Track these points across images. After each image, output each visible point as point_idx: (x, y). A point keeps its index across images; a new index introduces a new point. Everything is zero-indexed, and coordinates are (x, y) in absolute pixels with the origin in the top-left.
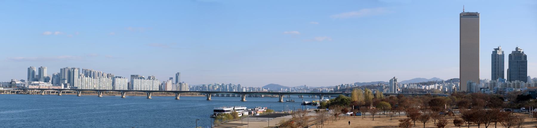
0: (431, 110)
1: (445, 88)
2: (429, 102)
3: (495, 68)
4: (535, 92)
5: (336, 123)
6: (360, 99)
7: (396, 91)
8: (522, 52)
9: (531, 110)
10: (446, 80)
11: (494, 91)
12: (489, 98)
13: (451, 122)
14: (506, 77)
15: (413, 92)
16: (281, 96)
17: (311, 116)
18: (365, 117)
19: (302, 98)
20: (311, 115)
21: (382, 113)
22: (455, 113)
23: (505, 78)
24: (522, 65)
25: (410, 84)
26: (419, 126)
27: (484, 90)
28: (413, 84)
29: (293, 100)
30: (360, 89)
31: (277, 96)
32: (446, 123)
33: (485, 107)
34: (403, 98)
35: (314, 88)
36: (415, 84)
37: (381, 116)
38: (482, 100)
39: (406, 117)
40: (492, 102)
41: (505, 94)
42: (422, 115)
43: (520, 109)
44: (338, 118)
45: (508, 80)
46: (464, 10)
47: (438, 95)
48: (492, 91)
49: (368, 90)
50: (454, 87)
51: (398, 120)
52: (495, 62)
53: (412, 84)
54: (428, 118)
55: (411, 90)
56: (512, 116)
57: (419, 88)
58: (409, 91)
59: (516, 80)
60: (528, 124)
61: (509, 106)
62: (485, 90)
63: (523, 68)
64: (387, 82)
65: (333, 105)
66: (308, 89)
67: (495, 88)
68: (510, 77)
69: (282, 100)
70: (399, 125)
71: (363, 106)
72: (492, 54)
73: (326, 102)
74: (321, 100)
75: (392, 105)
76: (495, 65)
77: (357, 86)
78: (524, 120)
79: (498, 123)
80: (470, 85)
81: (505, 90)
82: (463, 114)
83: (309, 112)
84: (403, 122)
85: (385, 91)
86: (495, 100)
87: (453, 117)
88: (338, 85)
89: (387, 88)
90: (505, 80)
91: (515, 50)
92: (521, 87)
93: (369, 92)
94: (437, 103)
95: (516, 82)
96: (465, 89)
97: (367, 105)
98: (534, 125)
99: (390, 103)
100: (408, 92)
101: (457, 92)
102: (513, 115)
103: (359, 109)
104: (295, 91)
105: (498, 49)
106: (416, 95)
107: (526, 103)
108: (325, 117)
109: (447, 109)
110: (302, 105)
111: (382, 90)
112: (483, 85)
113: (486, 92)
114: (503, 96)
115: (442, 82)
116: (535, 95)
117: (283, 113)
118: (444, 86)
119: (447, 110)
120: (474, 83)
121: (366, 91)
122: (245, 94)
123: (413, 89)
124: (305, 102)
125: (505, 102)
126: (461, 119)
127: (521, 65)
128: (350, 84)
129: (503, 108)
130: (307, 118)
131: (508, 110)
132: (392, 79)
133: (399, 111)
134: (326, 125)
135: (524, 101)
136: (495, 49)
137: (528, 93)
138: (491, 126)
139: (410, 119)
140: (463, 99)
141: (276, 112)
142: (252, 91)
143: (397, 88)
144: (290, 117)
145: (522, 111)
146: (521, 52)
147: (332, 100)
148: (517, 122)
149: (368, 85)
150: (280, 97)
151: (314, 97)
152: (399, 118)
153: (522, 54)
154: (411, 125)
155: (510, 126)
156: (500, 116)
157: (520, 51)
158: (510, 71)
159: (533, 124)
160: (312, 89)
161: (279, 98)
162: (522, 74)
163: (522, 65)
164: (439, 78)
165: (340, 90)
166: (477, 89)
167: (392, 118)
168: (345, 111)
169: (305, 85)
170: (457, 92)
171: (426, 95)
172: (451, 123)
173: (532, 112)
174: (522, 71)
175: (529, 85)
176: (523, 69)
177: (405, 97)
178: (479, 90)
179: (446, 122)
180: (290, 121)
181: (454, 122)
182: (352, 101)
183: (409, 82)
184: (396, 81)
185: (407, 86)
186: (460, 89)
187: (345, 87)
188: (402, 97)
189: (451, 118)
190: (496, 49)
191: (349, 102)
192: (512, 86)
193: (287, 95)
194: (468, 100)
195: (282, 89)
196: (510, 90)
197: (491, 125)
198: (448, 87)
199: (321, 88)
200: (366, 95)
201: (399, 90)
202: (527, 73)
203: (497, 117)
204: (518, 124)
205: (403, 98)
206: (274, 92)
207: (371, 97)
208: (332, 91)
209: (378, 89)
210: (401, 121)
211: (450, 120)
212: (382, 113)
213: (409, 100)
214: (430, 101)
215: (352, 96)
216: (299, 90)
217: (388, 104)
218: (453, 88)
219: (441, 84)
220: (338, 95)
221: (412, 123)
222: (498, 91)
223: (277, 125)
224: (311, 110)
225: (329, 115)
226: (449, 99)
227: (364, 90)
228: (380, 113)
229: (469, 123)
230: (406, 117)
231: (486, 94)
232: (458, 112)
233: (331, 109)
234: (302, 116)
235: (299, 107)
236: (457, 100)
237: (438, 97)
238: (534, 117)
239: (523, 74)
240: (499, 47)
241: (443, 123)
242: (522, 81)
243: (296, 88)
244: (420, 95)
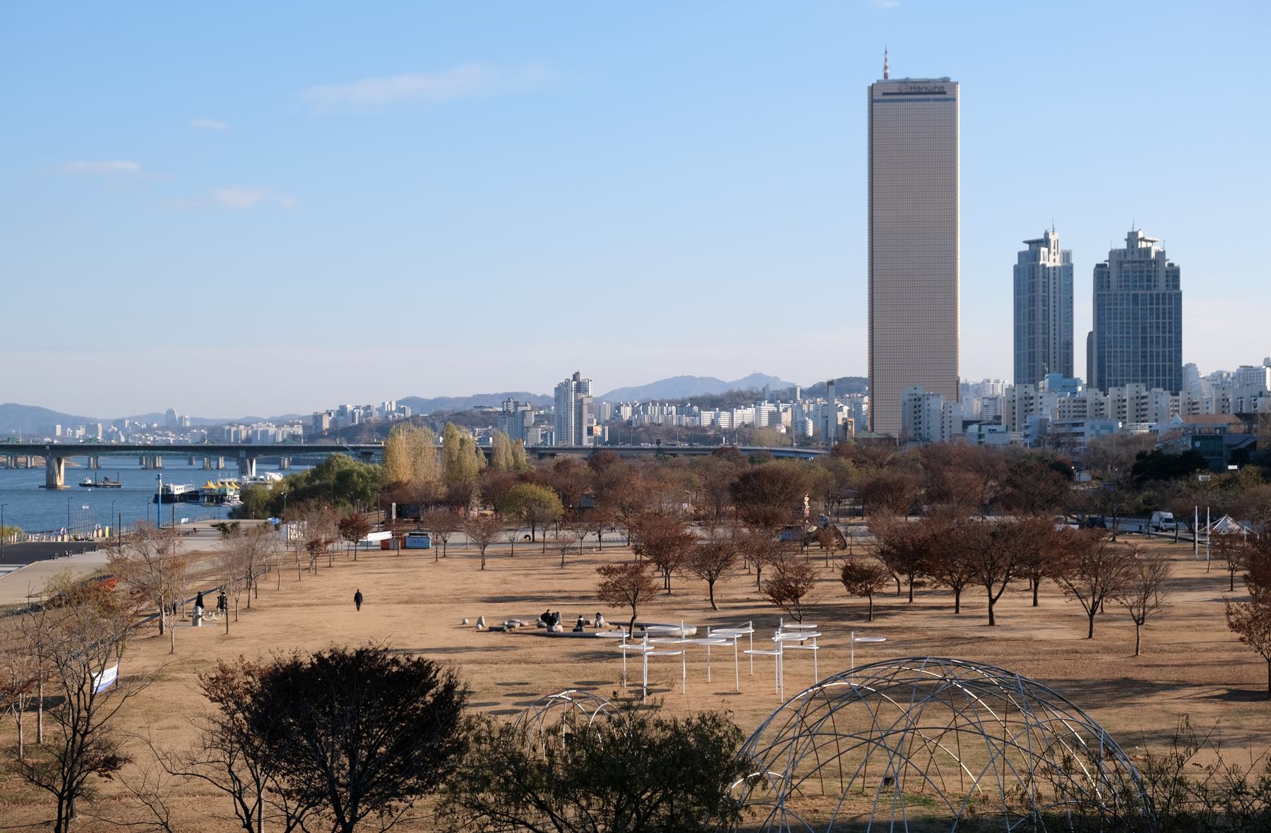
0: (740, 521)
1: (804, 424)
2: (732, 485)
3: (1032, 330)
4: (1220, 438)
5: (314, 585)
6: (423, 471)
7: (585, 437)
8: (1158, 253)
9: (1203, 521)
10: (806, 382)
11: (1026, 436)
12: (1002, 466)
13: (831, 576)
14: (1080, 369)
15: (658, 442)
16: (55, 461)
17: (197, 555)
18: (445, 556)
19: (155, 468)
20: (197, 548)
21: (524, 534)
22: (850, 535)
23: (1075, 376)
24: (1158, 314)
25: (645, 405)
26: (687, 594)
27: (980, 429)
28: (662, 404)
29: (113, 479)
30: (425, 428)
31: (37, 461)
32: (811, 580)
33: (986, 509)
34: (617, 468)
35: (213, 424)
36: (671, 403)
37: (517, 549)
38: (971, 476)
39: (629, 555)
40: (1015, 487)
41: (1077, 449)
42: (699, 543)
43: (1150, 518)
44: (322, 561)
45: (1089, 384)
46: (886, 68)
47: (773, 454)
48: (1016, 436)
49: (459, 429)
50: (842, 416)
51: (593, 567)
52: (1032, 302)
53: (654, 403)
54: (725, 559)
55: (652, 430)
56: (1113, 550)
57: (686, 420)
58: (644, 435)
59: (1128, 381)
60: (1190, 590)
61: (1097, 502)
62: (985, 429)
63: (1164, 328)
64: (544, 397)
65: (301, 500)
66: (185, 430)
67: (1033, 418)
68: (1101, 370)
69: (60, 482)
70: (599, 588)
71: (438, 503)
72: (1015, 267)
73: (270, 488)
74: (246, 479)
75: (565, 499)
76: (1032, 316)
77: (409, 413)
78: (1166, 570)
79: (1047, 583)
80: (916, 407)
81: (1144, 407)
82: (886, 542)
83: (187, 534)
84: (615, 578)
85: (536, 437)
86: (1030, 478)
87: (839, 553)
88: (322, 410)
89: (542, 422)
90: (1077, 382)
91: (1124, 246)
92: (1154, 417)
93: (462, 441)
94: (767, 491)
95: (1129, 391)
96: (892, 425)
97: (456, 499)
98: (1217, 595)
99: (557, 490)
100: (637, 440)
101: (856, 440)
102: (1119, 546)
103: (417, 520)
104: (123, 439)
105: (1045, 242)
106: (675, 455)
107: (1180, 491)
108: (265, 556)
109: (813, 519)
110: (156, 501)
111: (520, 431)
112: (974, 408)
113: (988, 439)
114: (1068, 456)
115: (788, 395)
116: (1221, 454)
117: (65, 541)
118: (799, 414)
119: (812, 521)
120: (932, 400)
121: (449, 437)
122: (66, 454)
123: (660, 425)
124: (168, 489)
125: (1079, 483)
126: (873, 562)
127: (1151, 313)
128: (376, 404)
129: (1068, 512)
130: (177, 564)
131: (1092, 523)
132: (567, 383)
133: (599, 524)
134: (271, 591)
135: (1167, 483)
136: (1030, 243)
137: (1186, 444)
138: (1014, 595)
139: (647, 562)
140: (885, 471)
141: (33, 539)
142: (123, 439)
143: (591, 421)
144: (99, 559)
145: (1157, 529)
146: (1153, 255)
147: (298, 479)
148: (1134, 577)
149: (460, 408)
150: (48, 464)
151: (214, 464)
152: (599, 557)
153: (1155, 262)
154: (651, 590)
155: (1101, 597)
156: (1054, 552)
157: (1148, 250)
158: (1098, 343)
159: (1211, 589)
160: (202, 427)
161: (48, 472)
162: (1158, 356)
163: (1158, 314)
164: (776, 379)
165: (333, 433)
166: (946, 425)
167: (568, 558)
168: (354, 529)
169: (171, 412)
170: (856, 440)
171: (719, 453)
172: (832, 580)
173: (1205, 535)
174: (1158, 343)
175: (1192, 407)
176: (1164, 332)
177: (627, 463)
178: (958, 428)
179: (808, 575)
180: (100, 579)
181: (843, 576)
182: (386, 484)
183: (643, 397)
184: (586, 391)
185: (635, 411)
186: (872, 424)
187: (353, 420)
188: (610, 461)
189: (833, 558)
190: (1036, 244)
191: (375, 485)
192: (1109, 410)
193: (86, 457)
194: (910, 476)
195: (59, 428)
196: (1103, 427)
197: (1012, 590)
198: (815, 418)
199: (247, 425)
200: (450, 454)
201: (598, 430)
202: (1180, 351)
203: (1041, 553)
204: (1139, 589)
205: (617, 468)
206: (21, 441)
207: (474, 463)
208: (294, 437)
209: (506, 428)
210: (608, 571)
211: (827, 567)
212: (520, 536)
213: (641, 475)
214: (736, 480)
215: (385, 461)
216: (143, 432)
217: (549, 495)
218: (840, 422)
219: (785, 402)
220: (321, 457)
221: (655, 582)
222: (1042, 435)
223: (36, 596)
224: (197, 526)
225: (282, 547)
226: (821, 471)
227: (442, 434)
228: (511, 534)
229: (911, 579)
230: (629, 555)
231: (987, 447)
232: (864, 528)
233: (293, 520)
234: (153, 554)
235: (141, 511)
236: (857, 476)
237: (773, 463)
238: (1215, 556)
239: (1164, 356)
240: (1046, 234)
241: (797, 582)
242: (1158, 386)
243: (127, 422)
244: (691, 452)
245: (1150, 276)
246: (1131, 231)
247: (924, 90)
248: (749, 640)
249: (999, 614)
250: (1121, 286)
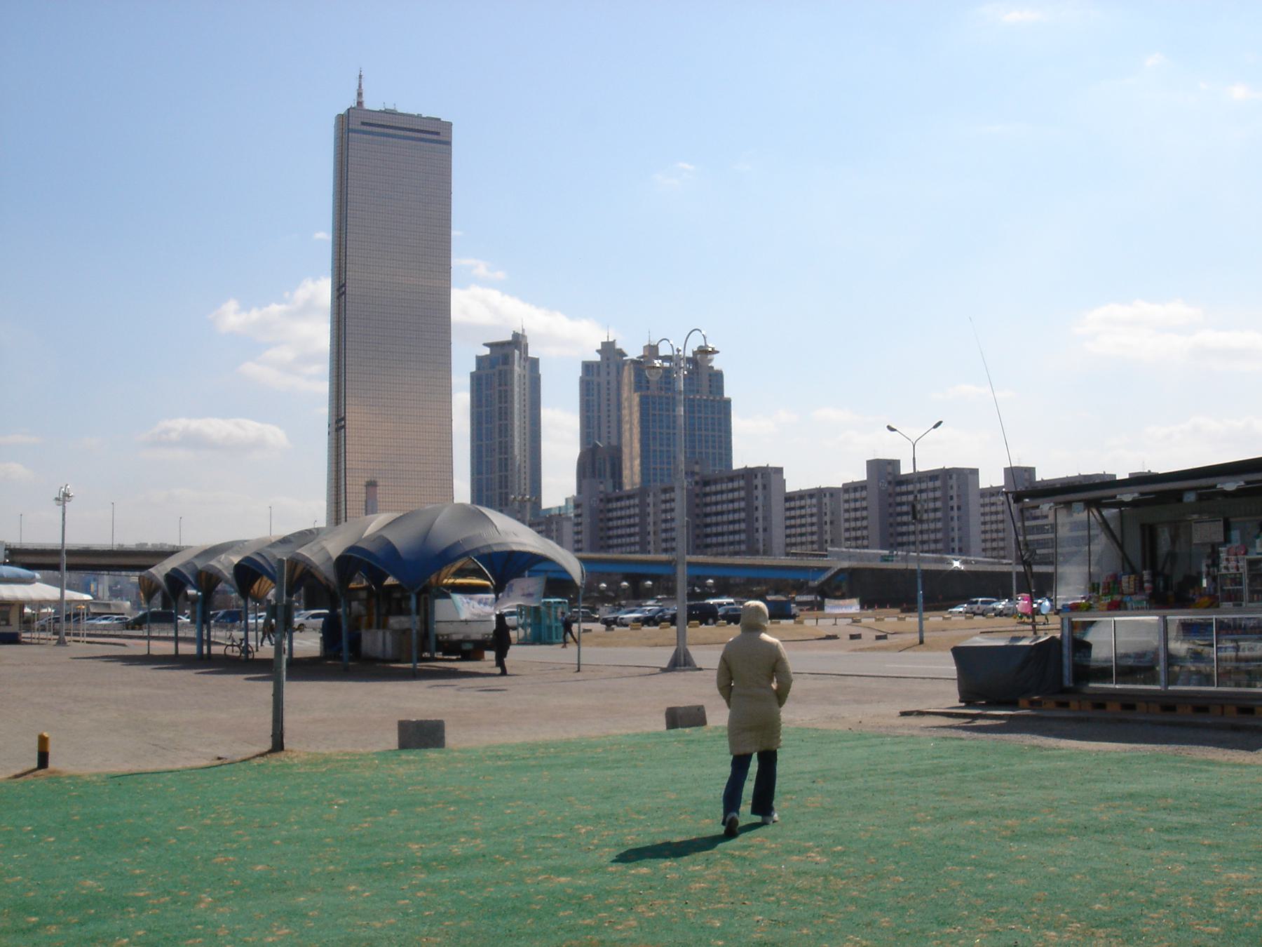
72: (472, 374)
164: (166, 544)
246: (606, 340)
248: (1213, 647)
249: (942, 686)
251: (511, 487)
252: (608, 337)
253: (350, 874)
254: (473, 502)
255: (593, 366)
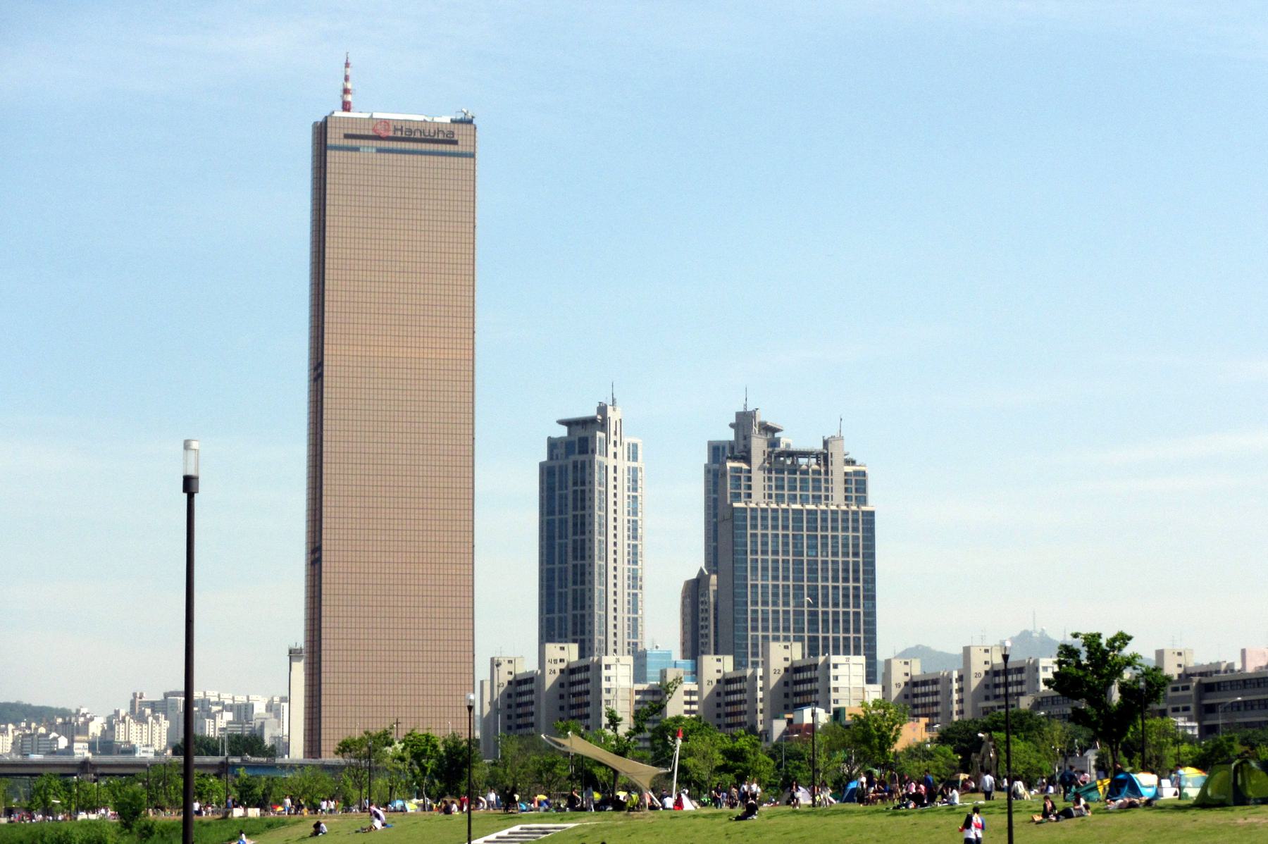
24: (835, 546)
46: (346, 91)
81: (525, 699)
136: (568, 423)
163: (835, 546)
240: (602, 409)
245: (819, 481)
246: (742, 410)
247: (418, 135)
250: (770, 496)
251: (590, 631)
252: (746, 405)
253: (912, 805)
254: (304, 757)
255: (724, 448)
